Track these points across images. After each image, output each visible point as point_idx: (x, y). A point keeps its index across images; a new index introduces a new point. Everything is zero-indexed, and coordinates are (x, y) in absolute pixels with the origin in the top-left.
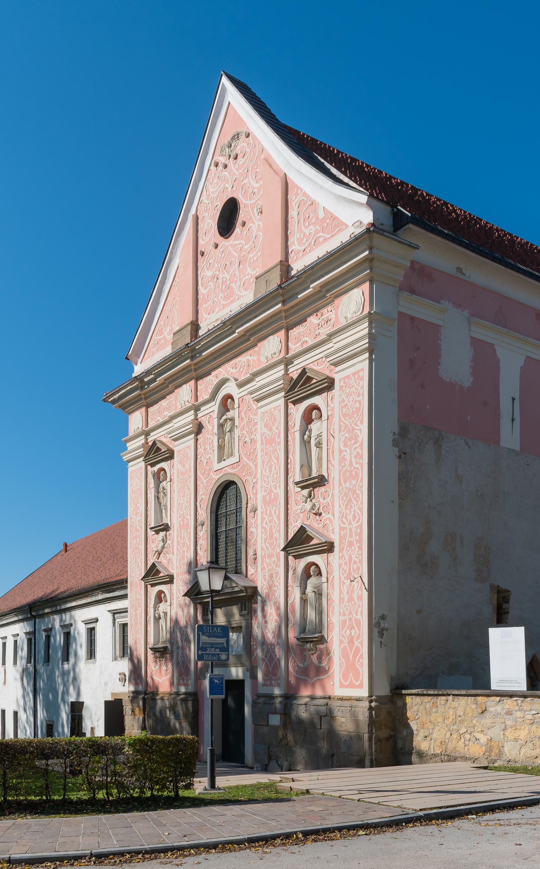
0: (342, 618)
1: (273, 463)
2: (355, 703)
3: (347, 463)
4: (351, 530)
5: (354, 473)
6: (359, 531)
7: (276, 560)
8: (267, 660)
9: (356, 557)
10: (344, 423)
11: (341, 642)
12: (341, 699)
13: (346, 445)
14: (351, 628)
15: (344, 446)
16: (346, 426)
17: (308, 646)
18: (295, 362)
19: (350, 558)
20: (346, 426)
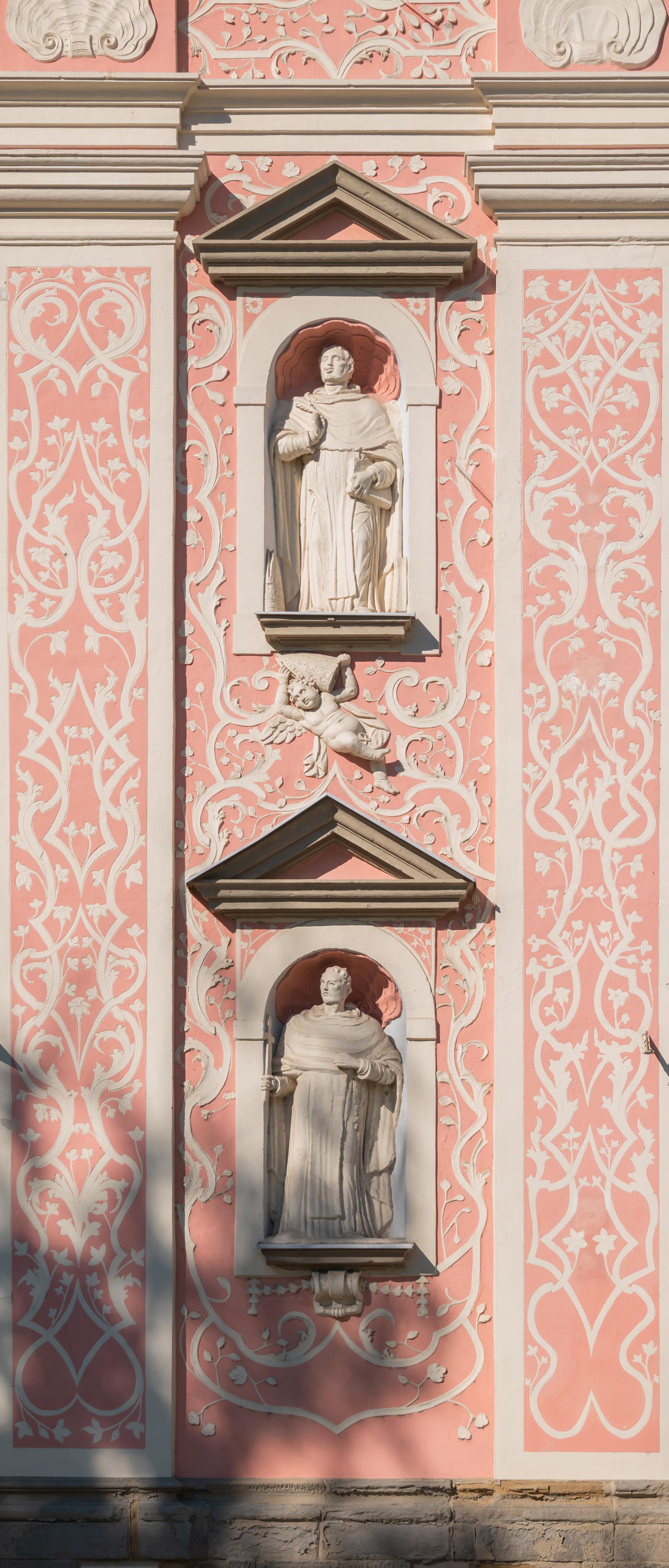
0: (536, 1184)
1: (92, 500)
2: (615, 1505)
3: (574, 601)
4: (592, 858)
5: (609, 648)
6: (637, 866)
7: (121, 918)
8: (48, 1336)
9: (621, 963)
10: (553, 446)
11: (534, 1277)
12: (540, 1493)
13: (560, 528)
14: (594, 1223)
15: (553, 533)
16: (564, 462)
17: (335, 1283)
18: (238, 122)
19: (590, 965)
20: (564, 462)
